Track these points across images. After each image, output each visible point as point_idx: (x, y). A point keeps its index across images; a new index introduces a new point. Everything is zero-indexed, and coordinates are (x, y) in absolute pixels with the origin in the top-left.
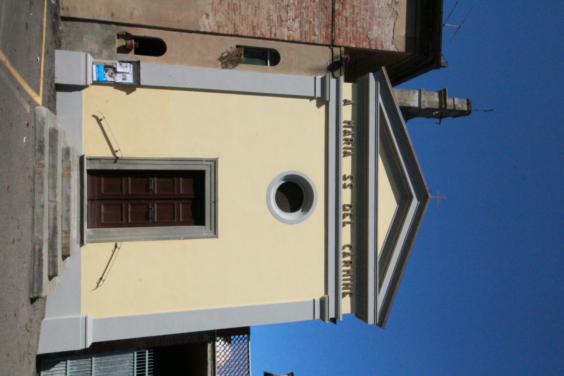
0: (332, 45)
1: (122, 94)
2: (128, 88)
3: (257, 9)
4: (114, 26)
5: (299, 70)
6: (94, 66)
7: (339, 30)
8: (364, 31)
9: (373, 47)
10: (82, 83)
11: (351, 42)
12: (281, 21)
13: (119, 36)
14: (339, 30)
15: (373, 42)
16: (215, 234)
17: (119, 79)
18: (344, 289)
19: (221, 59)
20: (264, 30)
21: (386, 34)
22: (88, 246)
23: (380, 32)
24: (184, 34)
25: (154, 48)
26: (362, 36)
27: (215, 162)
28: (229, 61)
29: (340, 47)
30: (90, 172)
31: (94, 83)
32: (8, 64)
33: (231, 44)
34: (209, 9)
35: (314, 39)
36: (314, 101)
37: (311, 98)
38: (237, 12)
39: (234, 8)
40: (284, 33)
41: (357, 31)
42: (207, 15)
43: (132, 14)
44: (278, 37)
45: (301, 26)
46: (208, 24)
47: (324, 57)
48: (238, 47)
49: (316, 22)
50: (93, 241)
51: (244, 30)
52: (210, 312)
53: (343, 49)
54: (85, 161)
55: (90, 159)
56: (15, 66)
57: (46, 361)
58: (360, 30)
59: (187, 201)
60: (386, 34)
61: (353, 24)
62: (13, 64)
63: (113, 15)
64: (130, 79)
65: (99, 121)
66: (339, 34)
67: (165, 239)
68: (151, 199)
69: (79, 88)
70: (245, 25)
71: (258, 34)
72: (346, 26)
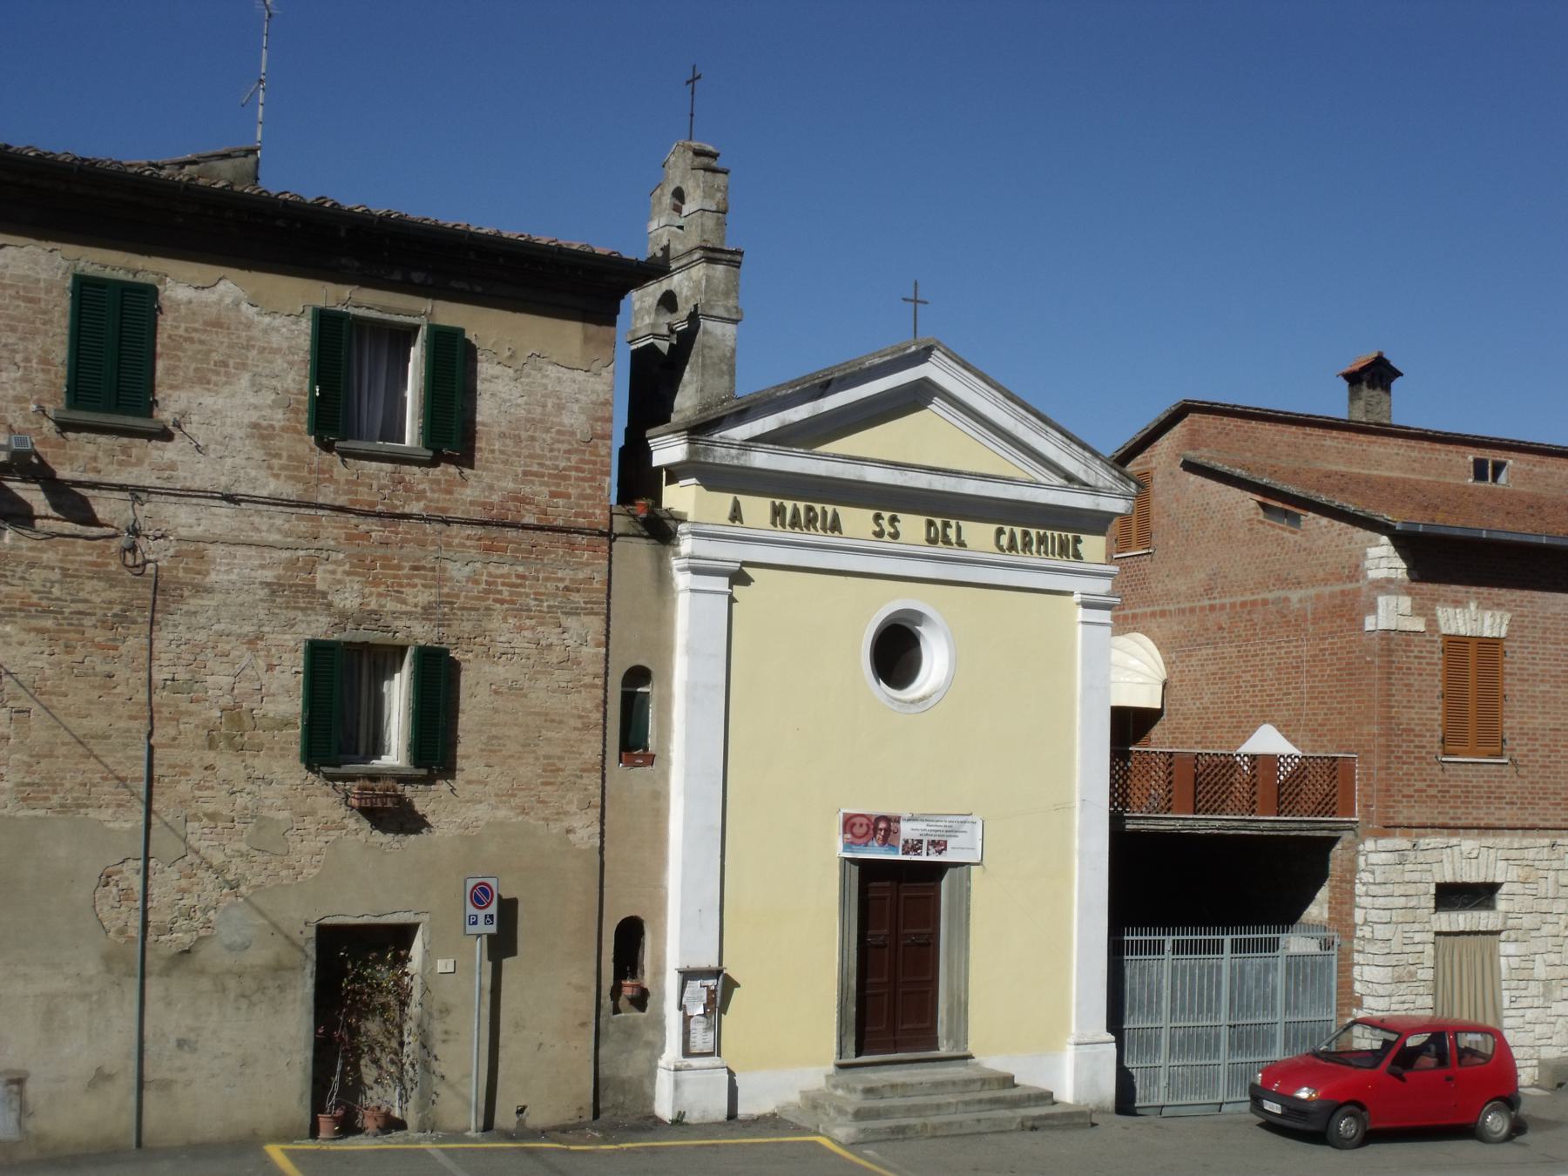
8: (577, 451)
12: (568, 661)
20: (587, 701)
23: (576, 407)
26: (587, 457)
35: (600, 577)
38: (559, 764)
40: (592, 652)
41: (577, 469)
42: (568, 831)
43: (579, 988)
45: (574, 612)
47: (635, 552)
54: (844, 1061)
58: (574, 458)
63: (583, 1025)
70: (583, 748)
72: (568, 496)
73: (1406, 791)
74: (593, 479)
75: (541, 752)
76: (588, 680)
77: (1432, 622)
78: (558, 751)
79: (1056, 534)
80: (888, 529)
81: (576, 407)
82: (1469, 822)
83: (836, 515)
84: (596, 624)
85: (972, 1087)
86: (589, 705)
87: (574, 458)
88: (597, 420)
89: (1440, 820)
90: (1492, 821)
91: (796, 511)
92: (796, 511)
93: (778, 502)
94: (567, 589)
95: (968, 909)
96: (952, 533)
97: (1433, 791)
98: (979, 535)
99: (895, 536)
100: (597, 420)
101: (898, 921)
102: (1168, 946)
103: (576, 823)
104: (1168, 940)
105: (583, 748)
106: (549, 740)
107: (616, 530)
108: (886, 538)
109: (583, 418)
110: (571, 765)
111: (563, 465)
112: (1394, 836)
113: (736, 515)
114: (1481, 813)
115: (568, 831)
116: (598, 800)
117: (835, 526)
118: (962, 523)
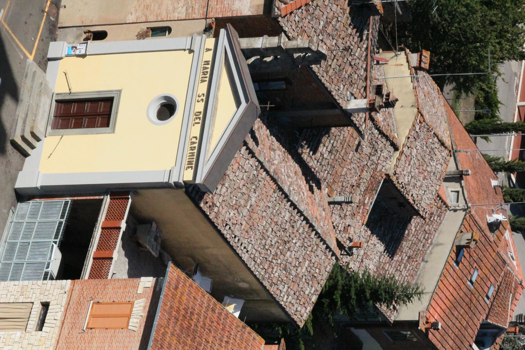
0: (206, 18)
1: (81, 59)
2: (83, 56)
3: (160, 5)
4: (83, 28)
5: (183, 35)
6: (67, 48)
7: (212, 8)
8: (229, 6)
9: (235, 15)
10: (59, 56)
11: (219, 14)
12: (174, 9)
13: (85, 33)
14: (212, 8)
15: (234, 12)
16: (113, 132)
17: (77, 52)
18: (188, 164)
19: (137, 36)
20: (164, 17)
21: (244, 6)
22: (48, 138)
23: (240, 5)
24: (115, 23)
25: (100, 36)
26: (227, 9)
27: (120, 91)
28: (142, 36)
29: (211, 18)
30: (57, 101)
31: (66, 56)
32: (10, 32)
33: (144, 27)
34: (133, 10)
35: (195, 16)
36: (187, 51)
37: (185, 50)
38: (149, 9)
39: (147, 7)
40: (176, 16)
41: (224, 7)
42: (131, 14)
43: (92, 20)
44: (171, 19)
45: (187, 10)
46: (131, 18)
47: (202, 25)
48: (148, 28)
49: (197, 6)
50: (51, 135)
51: (151, 18)
52: (77, 134)
53: (213, 19)
54: (54, 95)
55: (57, 94)
56: (15, 35)
57: (22, 196)
58: (227, 6)
59: (105, 116)
60: (244, 6)
61: (222, 4)
62: (13, 33)
63: (82, 22)
64: (83, 52)
65: (66, 74)
66: (212, 10)
67: (86, 134)
68: (85, 116)
69: (60, 59)
70: (152, 16)
71: (159, 19)
72: (217, 5)
73: (85, 288)
74: (221, 12)
75: (152, 4)
76: (169, 15)
77: (139, 296)
78: (152, 8)
79: (194, 160)
80: (200, 99)
81: (240, 5)
82: (67, 315)
83: (206, 81)
84: (183, 17)
85: (34, 116)
86: (163, 16)
87: (227, 6)
88: (237, 12)
89: (71, 303)
90: (65, 325)
91: (208, 68)
92: (208, 68)
93: (210, 63)
94: (193, 7)
95: (88, 134)
96: (197, 121)
97: (81, 299)
98: (196, 131)
99: (198, 101)
100: (237, 12)
101: (89, 112)
102: (62, 220)
103: (134, 15)
104: (64, 220)
105: (152, 16)
106: (155, 6)
107: (208, 20)
108: (197, 98)
109: (237, 7)
110: (148, 13)
111: (225, 3)
112: (71, 285)
113: (208, 50)
114: (69, 320)
115: (131, 14)
116: (138, 21)
117: (203, 81)
118: (200, 124)
